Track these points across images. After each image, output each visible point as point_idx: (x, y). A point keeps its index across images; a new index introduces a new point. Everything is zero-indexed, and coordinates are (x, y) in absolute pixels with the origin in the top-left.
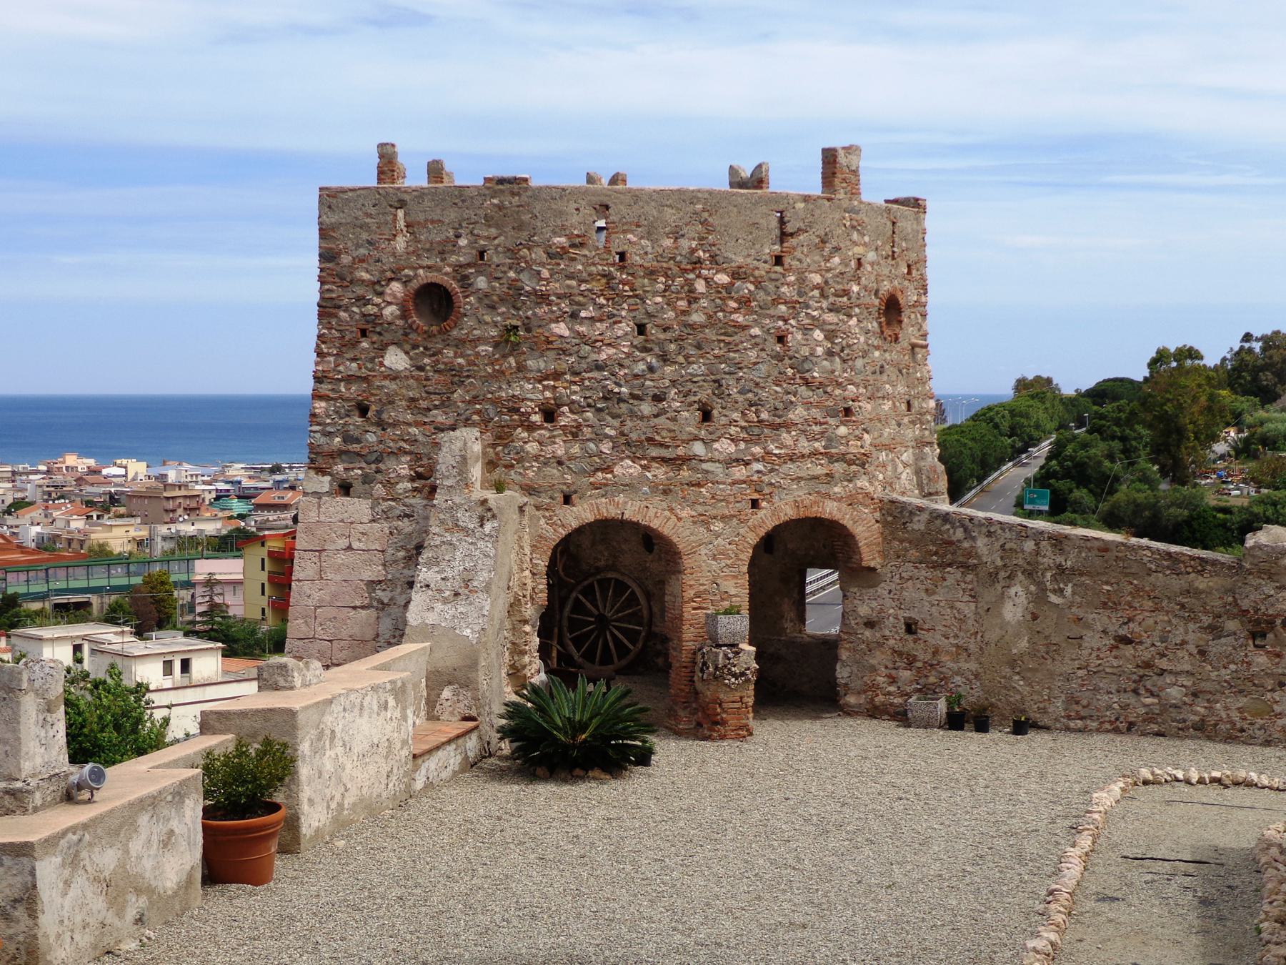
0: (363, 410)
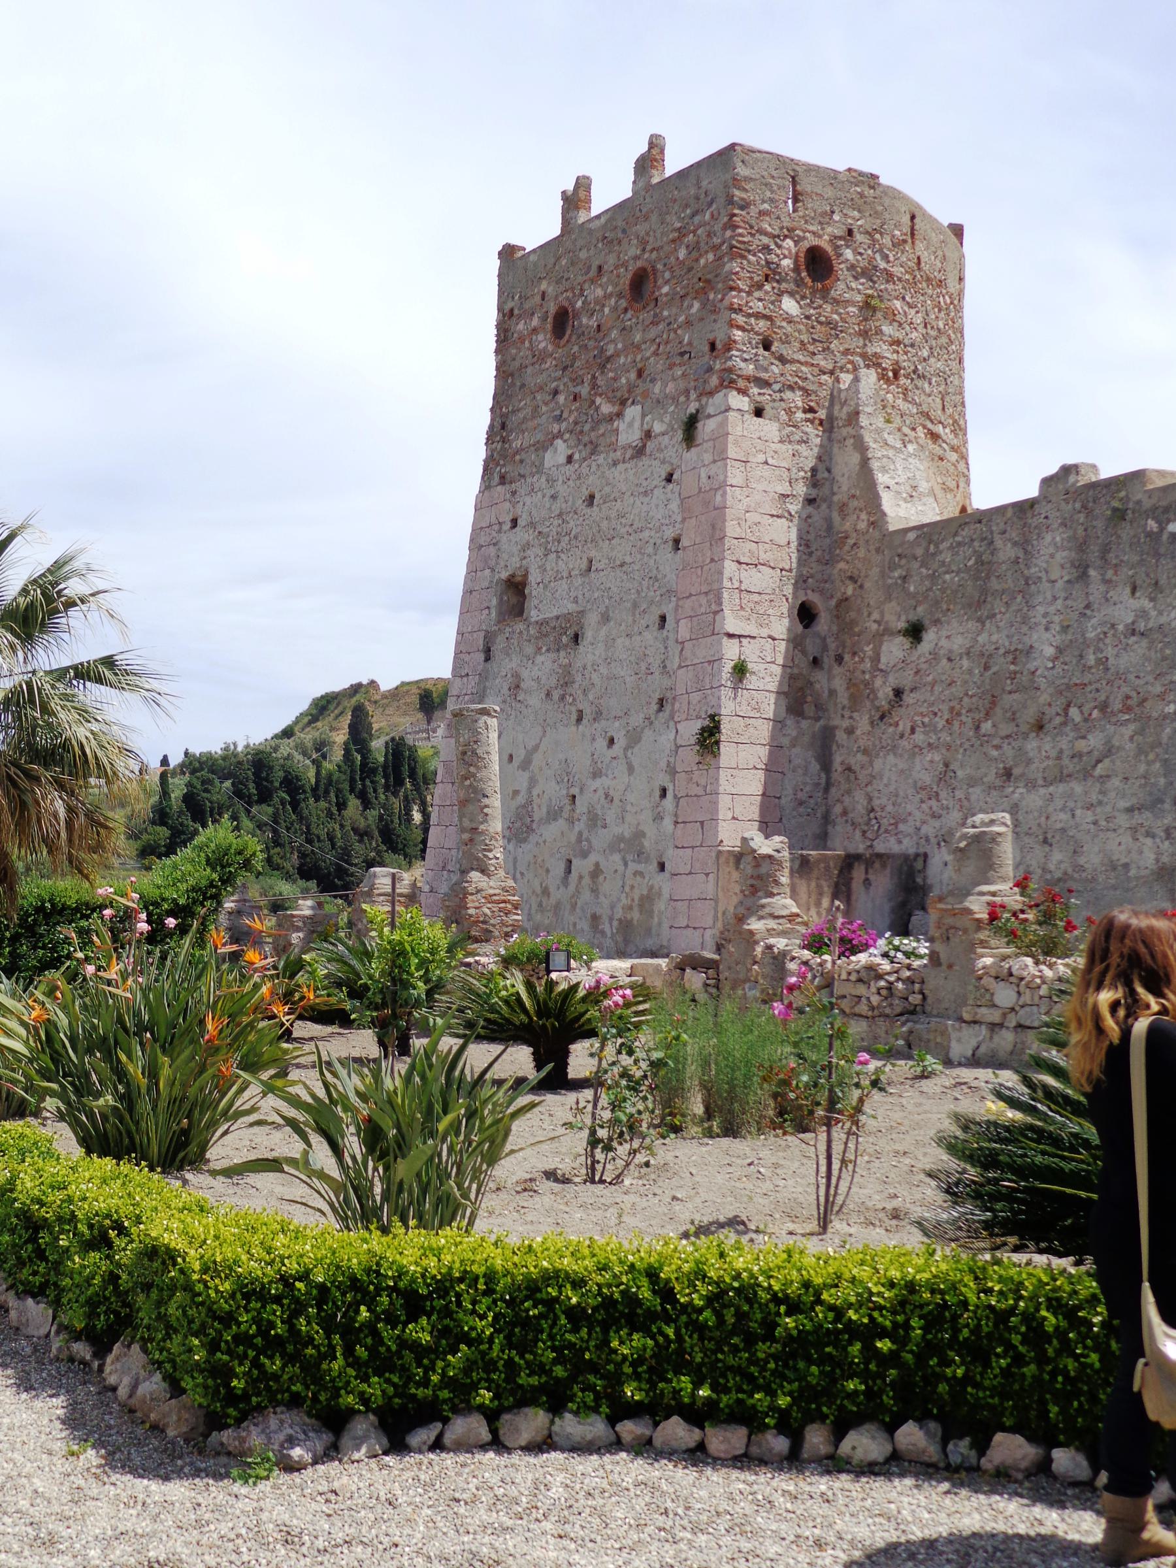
0: (767, 346)
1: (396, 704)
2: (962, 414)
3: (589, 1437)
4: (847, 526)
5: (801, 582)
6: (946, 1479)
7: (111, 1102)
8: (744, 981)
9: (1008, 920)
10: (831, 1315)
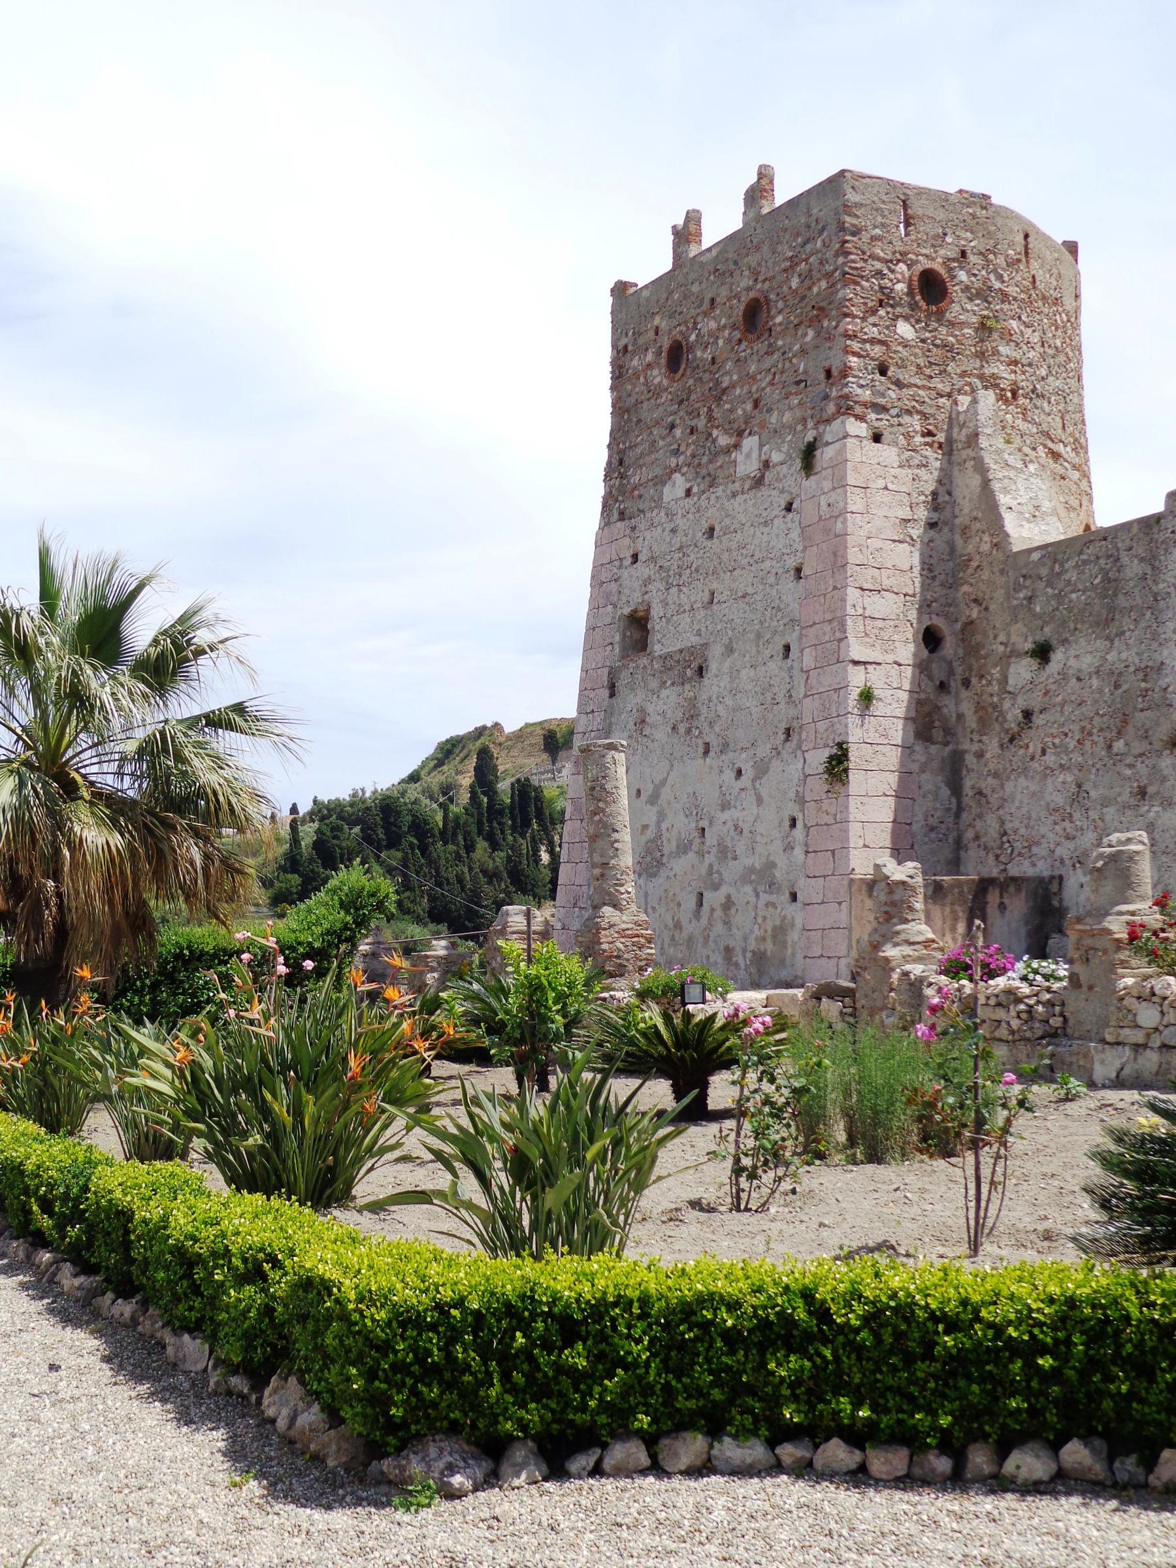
0: (883, 371)
1: (520, 745)
2: (1083, 432)
3: (749, 1461)
4: (970, 548)
5: (925, 607)
6: (1114, 1497)
7: (260, 1142)
8: (882, 1009)
9: (1148, 939)
10: (990, 1333)
